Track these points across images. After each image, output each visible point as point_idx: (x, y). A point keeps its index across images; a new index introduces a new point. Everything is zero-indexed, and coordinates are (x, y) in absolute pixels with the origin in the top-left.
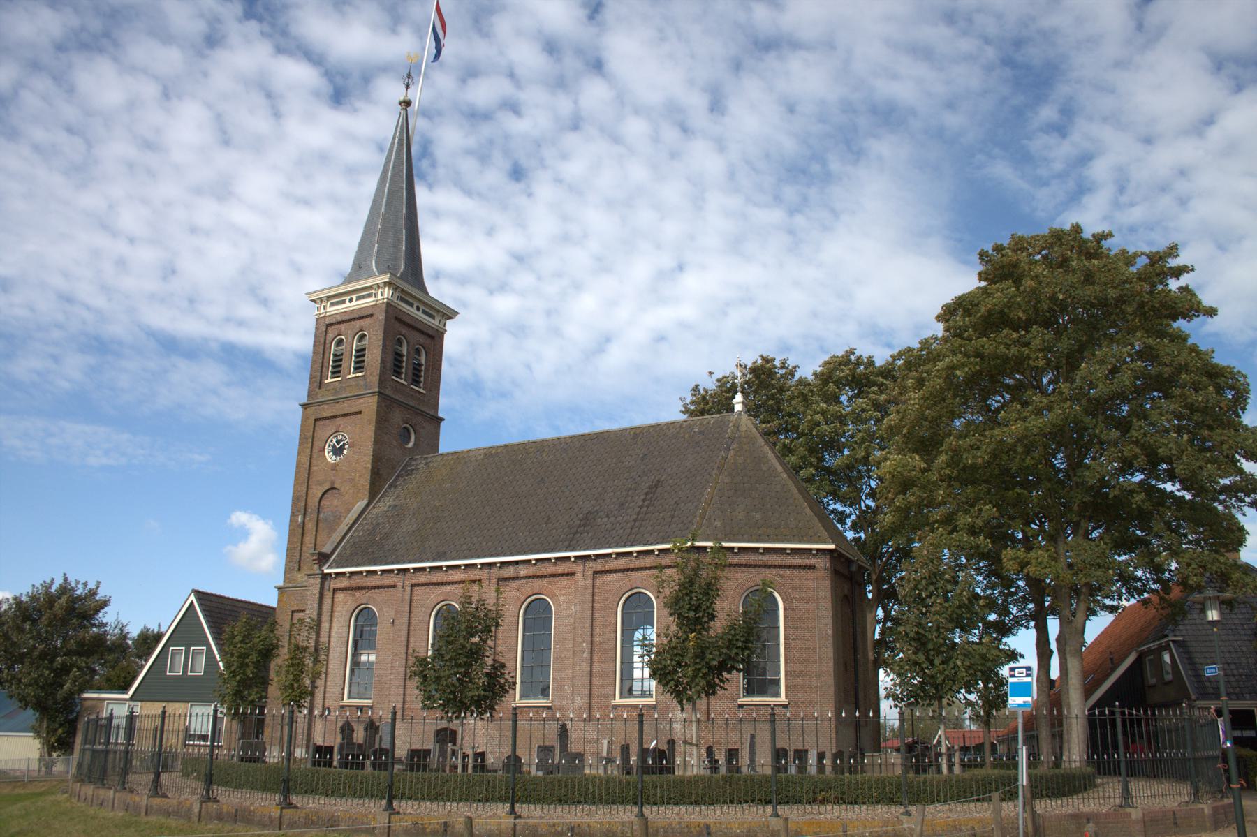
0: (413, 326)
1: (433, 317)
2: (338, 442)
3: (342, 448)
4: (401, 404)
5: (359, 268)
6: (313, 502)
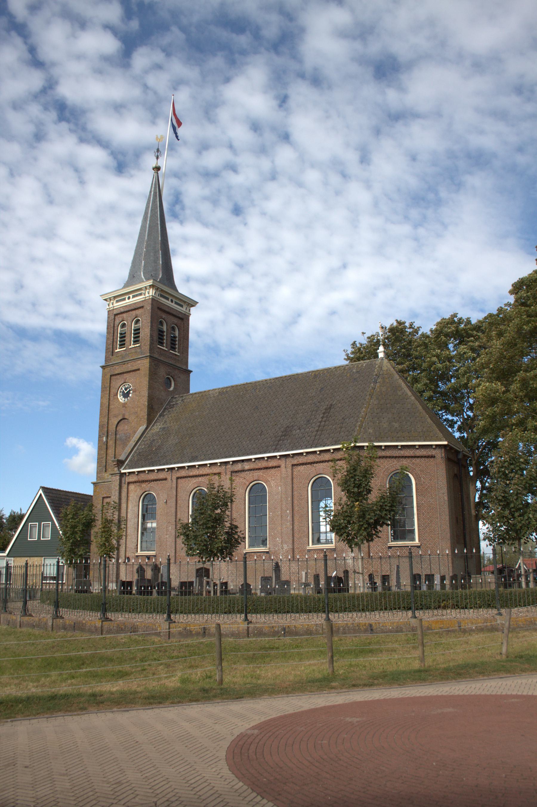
1: (182, 306)
2: (126, 389)
3: (128, 393)
5: (133, 278)
6: (112, 428)
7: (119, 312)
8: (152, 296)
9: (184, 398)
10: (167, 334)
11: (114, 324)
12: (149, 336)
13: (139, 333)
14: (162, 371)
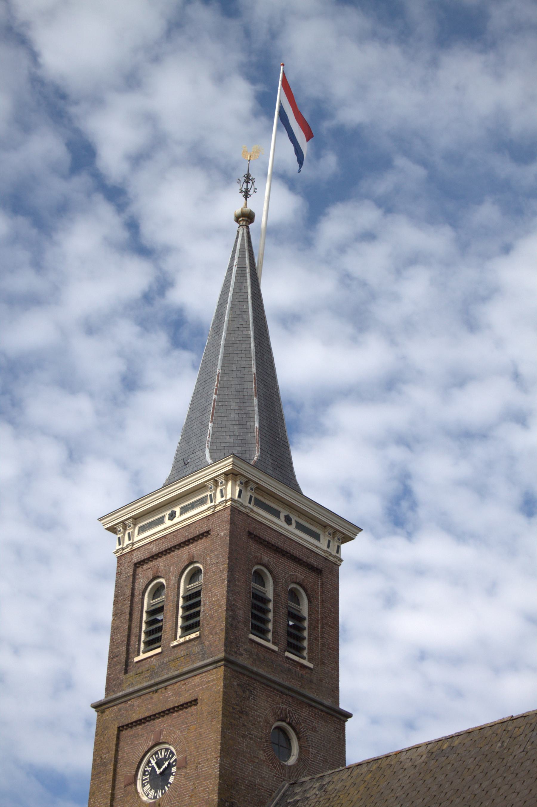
0: (282, 550)
1: (317, 537)
2: (159, 764)
3: (166, 773)
4: (268, 684)
5: (184, 464)
7: (147, 555)
8: (232, 500)
9: (327, 780)
10: (275, 607)
11: (133, 589)
12: (224, 607)
13: (198, 604)
14: (263, 708)
